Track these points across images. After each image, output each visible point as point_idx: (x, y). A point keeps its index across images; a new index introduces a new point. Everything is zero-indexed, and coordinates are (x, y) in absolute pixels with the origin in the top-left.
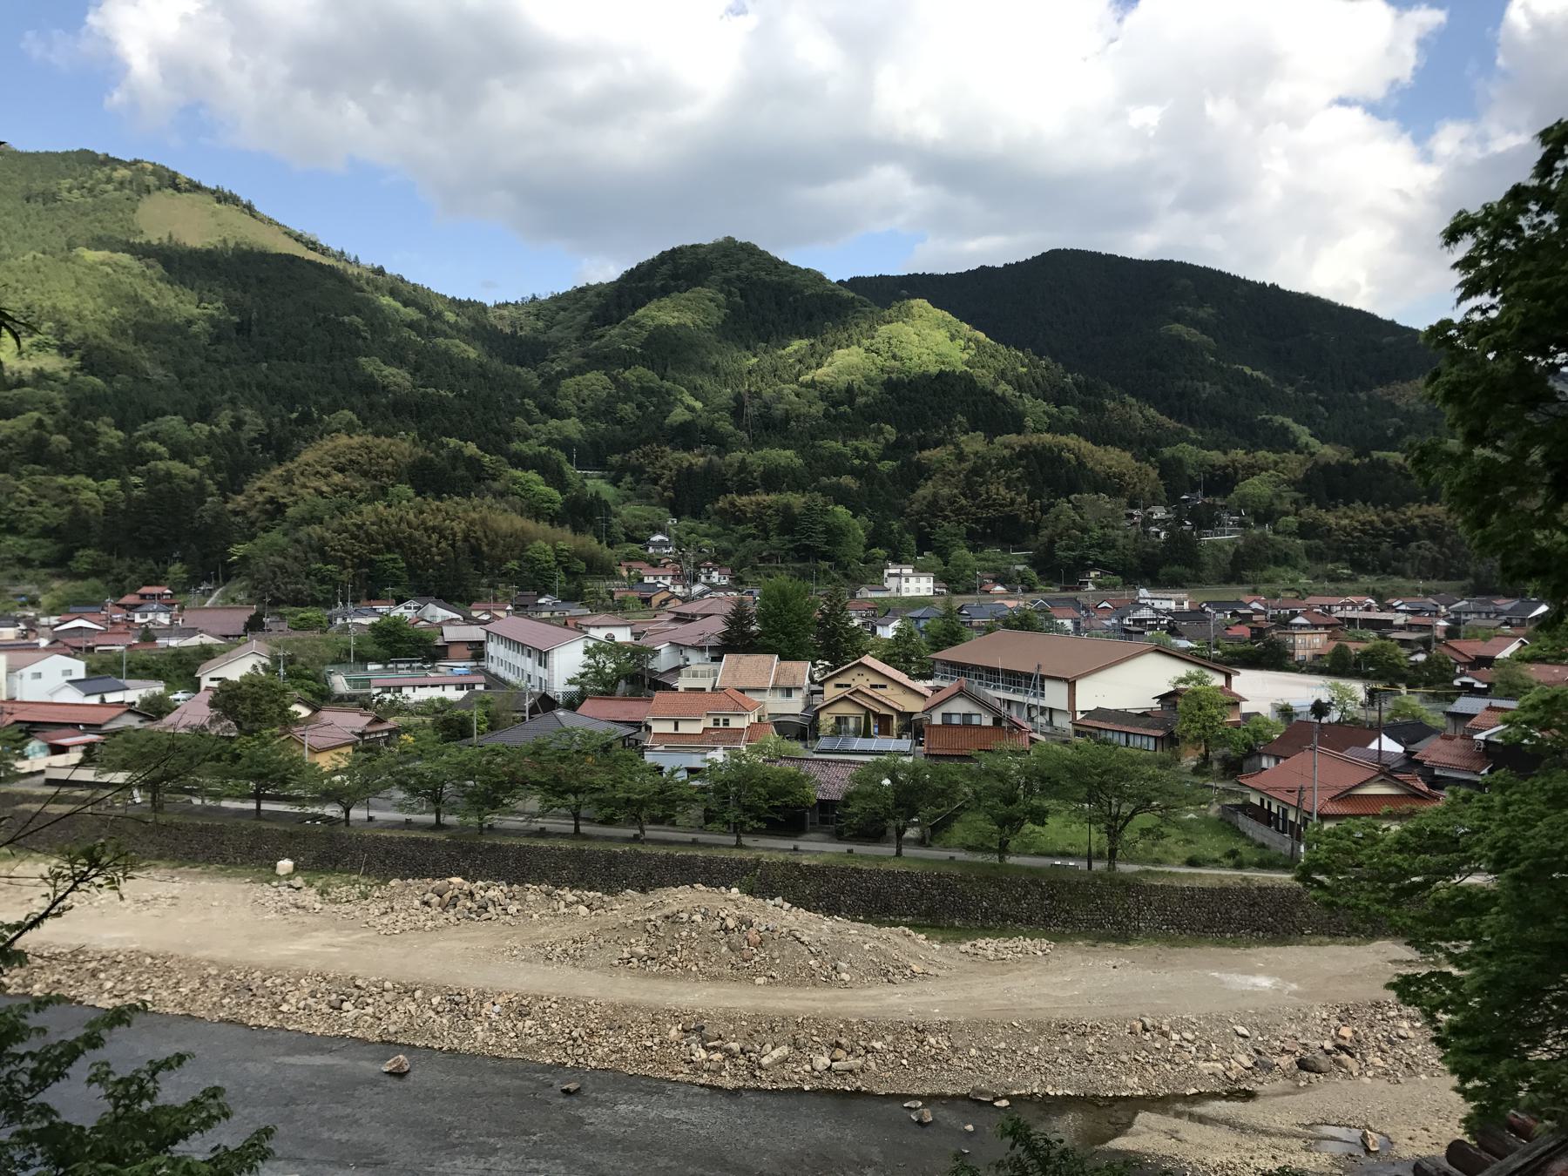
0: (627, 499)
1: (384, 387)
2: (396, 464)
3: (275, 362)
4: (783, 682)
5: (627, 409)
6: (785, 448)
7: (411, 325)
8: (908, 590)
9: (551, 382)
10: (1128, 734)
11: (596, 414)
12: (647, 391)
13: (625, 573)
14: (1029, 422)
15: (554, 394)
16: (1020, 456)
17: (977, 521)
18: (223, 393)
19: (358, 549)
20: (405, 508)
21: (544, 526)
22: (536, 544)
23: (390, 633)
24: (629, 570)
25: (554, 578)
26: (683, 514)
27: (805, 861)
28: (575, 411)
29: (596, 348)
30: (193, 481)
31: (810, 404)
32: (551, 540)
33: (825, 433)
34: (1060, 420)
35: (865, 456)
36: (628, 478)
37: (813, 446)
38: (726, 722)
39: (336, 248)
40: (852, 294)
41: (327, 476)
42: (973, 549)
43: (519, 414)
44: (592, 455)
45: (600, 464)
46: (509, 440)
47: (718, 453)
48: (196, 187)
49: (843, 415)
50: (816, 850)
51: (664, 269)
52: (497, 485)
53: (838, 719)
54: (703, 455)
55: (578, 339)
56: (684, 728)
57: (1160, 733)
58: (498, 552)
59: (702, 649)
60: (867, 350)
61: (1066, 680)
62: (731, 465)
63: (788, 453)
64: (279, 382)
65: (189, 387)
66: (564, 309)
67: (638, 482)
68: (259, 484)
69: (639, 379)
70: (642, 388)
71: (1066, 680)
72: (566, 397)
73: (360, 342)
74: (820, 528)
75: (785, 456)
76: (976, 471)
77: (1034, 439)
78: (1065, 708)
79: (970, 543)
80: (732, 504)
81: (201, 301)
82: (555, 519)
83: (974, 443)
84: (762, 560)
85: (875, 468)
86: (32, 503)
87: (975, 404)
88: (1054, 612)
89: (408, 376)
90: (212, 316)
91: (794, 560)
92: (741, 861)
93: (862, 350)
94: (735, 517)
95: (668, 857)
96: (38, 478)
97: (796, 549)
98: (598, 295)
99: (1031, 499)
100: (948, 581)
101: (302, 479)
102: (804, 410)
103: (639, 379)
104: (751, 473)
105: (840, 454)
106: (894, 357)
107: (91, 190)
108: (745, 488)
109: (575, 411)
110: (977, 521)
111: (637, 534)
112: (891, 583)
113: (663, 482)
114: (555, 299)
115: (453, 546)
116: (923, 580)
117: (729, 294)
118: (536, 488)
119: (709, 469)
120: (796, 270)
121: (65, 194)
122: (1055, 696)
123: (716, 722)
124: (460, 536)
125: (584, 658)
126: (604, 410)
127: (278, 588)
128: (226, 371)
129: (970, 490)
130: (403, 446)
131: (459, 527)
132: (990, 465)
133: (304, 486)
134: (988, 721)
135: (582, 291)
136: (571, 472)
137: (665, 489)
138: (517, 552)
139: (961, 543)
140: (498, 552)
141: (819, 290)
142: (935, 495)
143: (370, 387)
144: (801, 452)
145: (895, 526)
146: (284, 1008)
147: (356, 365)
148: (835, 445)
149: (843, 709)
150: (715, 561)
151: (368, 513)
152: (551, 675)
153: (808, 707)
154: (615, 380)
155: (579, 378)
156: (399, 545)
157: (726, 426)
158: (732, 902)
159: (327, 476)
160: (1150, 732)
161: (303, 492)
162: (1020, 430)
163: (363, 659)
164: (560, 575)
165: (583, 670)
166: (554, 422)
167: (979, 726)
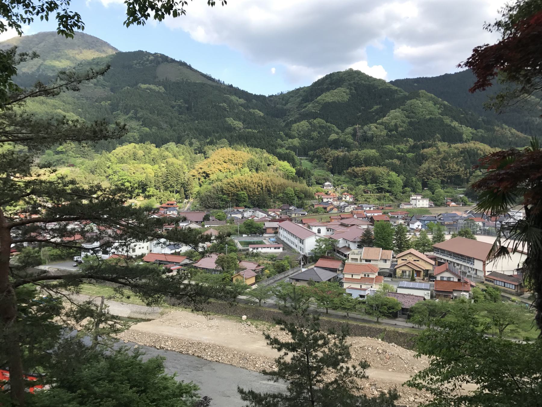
0: (315, 167)
1: (234, 128)
3: (200, 121)
4: (384, 258)
5: (315, 134)
7: (242, 105)
8: (419, 205)
9: (288, 125)
10: (505, 283)
12: (322, 127)
13: (317, 197)
14: (464, 136)
16: (462, 152)
17: (445, 177)
18: (185, 132)
19: (234, 190)
21: (290, 182)
23: (250, 225)
24: (318, 196)
25: (294, 199)
26: (335, 173)
27: (400, 330)
28: (297, 135)
29: (304, 112)
31: (381, 131)
34: (476, 135)
35: (402, 151)
36: (316, 160)
37: (383, 148)
38: (368, 275)
39: (217, 79)
40: (396, 88)
42: (443, 188)
44: (303, 152)
45: (306, 155)
46: (276, 148)
47: (348, 151)
48: (173, 61)
50: (402, 325)
51: (328, 81)
53: (403, 272)
54: (342, 151)
55: (297, 108)
56: (354, 277)
57: (517, 284)
58: (276, 191)
59: (355, 242)
60: (403, 110)
61: (482, 261)
62: (352, 155)
63: (374, 151)
64: (201, 127)
65: (174, 130)
66: (292, 97)
67: (319, 161)
69: (319, 123)
71: (482, 261)
72: (294, 131)
73: (226, 112)
74: (386, 181)
75: (372, 152)
76: (444, 158)
77: (466, 145)
78: (482, 270)
79: (442, 185)
80: (353, 170)
81: (176, 99)
82: (293, 179)
83: (443, 146)
85: (406, 156)
86: (134, 173)
87: (443, 130)
88: (475, 219)
91: (377, 193)
92: (380, 329)
93: (400, 110)
94: (355, 175)
95: (357, 325)
96: (136, 165)
97: (377, 189)
98: (304, 91)
99: (466, 169)
100: (433, 201)
103: (319, 123)
104: (360, 159)
105: (392, 151)
106: (413, 112)
107: (142, 64)
108: (358, 165)
109: (297, 135)
110: (445, 177)
111: (320, 182)
112: (413, 202)
113: (328, 162)
114: (289, 93)
115: (262, 189)
116: (425, 201)
117: (351, 89)
119: (344, 157)
120: (375, 80)
121: (135, 66)
122: (478, 265)
123: (365, 275)
124: (264, 186)
125: (316, 243)
126: (306, 135)
127: (209, 203)
128: (185, 124)
129: (442, 166)
131: (264, 182)
132: (450, 156)
134: (456, 280)
135: (298, 90)
136: (297, 158)
137: (329, 164)
138: (282, 191)
139: (439, 185)
141: (384, 87)
142: (429, 167)
143: (230, 129)
144: (378, 150)
145: (414, 179)
146: (257, 366)
147: (225, 121)
148: (390, 147)
149: (405, 268)
150: (347, 192)
152: (305, 246)
153: (393, 265)
154: (310, 123)
155: (298, 124)
156: (245, 189)
157: (350, 140)
158: (378, 343)
160: (513, 283)
162: (461, 141)
163: (241, 233)
164: (296, 198)
165: (316, 247)
166: (290, 140)
167: (453, 281)
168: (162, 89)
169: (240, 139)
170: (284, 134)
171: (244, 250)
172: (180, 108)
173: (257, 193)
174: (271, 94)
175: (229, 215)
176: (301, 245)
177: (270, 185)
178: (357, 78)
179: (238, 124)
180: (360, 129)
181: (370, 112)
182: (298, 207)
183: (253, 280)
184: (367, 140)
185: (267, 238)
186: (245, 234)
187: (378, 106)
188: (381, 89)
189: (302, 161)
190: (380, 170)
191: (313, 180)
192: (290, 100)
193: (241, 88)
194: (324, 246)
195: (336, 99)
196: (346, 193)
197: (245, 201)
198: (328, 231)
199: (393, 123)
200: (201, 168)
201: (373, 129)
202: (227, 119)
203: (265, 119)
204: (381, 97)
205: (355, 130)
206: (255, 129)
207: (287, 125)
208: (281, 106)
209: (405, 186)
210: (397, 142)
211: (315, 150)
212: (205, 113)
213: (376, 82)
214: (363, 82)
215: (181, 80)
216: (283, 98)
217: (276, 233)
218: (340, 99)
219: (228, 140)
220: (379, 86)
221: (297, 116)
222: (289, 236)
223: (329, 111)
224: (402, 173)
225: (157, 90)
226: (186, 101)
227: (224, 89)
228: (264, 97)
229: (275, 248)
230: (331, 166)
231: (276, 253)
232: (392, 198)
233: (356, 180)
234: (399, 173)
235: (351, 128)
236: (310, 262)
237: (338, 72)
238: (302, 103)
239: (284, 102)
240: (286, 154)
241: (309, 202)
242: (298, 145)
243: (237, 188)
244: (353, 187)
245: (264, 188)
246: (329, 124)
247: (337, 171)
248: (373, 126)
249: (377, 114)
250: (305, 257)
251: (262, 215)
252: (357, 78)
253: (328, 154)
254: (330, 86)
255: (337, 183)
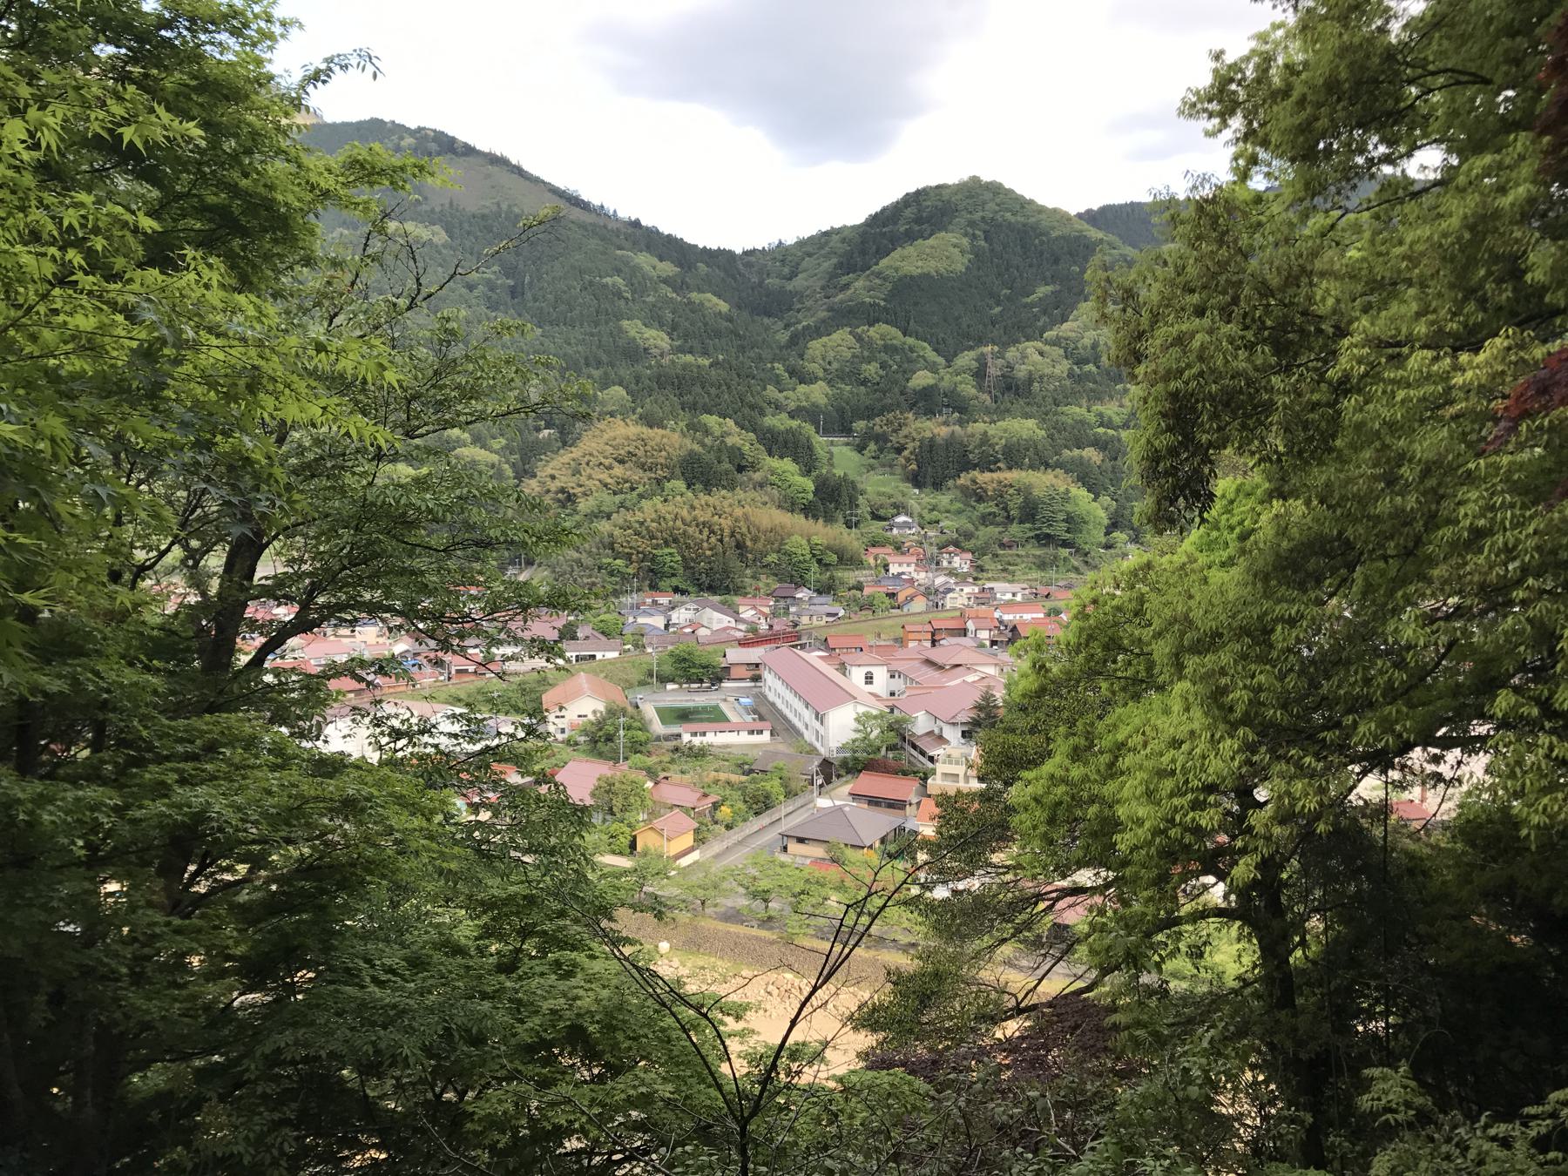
0: (872, 468)
2: (669, 457)
5: (871, 370)
6: (1027, 416)
7: (665, 281)
11: (842, 376)
12: (890, 349)
13: (872, 561)
15: (801, 356)
19: (643, 545)
20: (679, 505)
21: (799, 520)
22: (793, 538)
23: (685, 660)
29: (841, 302)
30: (493, 466)
32: (806, 533)
33: (1068, 397)
35: (1108, 424)
36: (872, 446)
37: (1056, 414)
39: (596, 202)
41: (610, 468)
43: (770, 381)
44: (838, 422)
45: (846, 430)
46: (762, 414)
47: (961, 422)
48: (469, 151)
49: (1088, 377)
51: (908, 212)
52: (757, 476)
54: (946, 423)
55: (823, 288)
58: (760, 545)
62: (973, 435)
63: (1031, 423)
66: (810, 255)
68: (549, 471)
70: (885, 346)
73: (622, 302)
74: (1061, 516)
75: (1025, 428)
80: (974, 481)
82: (809, 510)
84: (1002, 546)
85: (1119, 440)
89: (666, 337)
90: (490, 280)
98: (843, 240)
101: (589, 471)
102: (1048, 371)
105: (1082, 422)
108: (988, 464)
111: (882, 512)
113: (906, 453)
114: (801, 243)
115: (721, 541)
117: (974, 237)
118: (790, 478)
119: (951, 442)
120: (1042, 210)
124: (727, 532)
125: (855, 725)
126: (848, 373)
130: (673, 440)
131: (726, 523)
133: (590, 477)
136: (820, 441)
137: (907, 460)
140: (760, 545)
141: (1066, 231)
143: (635, 353)
147: (620, 330)
148: (1076, 411)
151: (649, 509)
152: (827, 729)
154: (859, 339)
155: (825, 339)
156: (675, 541)
157: (968, 389)
159: (610, 468)
161: (589, 483)
163: (664, 680)
164: (815, 567)
166: (802, 388)
168: (440, 236)
169: (661, 386)
170: (786, 370)
171: (667, 738)
172: (492, 290)
173: (708, 553)
174: (749, 247)
175: (631, 619)
176: (817, 725)
177: (744, 530)
178: (991, 206)
179: (657, 339)
180: (996, 356)
181: (1026, 305)
182: (819, 592)
183: (688, 840)
184: (1014, 391)
185: (730, 698)
186: (673, 681)
187: (1050, 288)
188: (1056, 238)
189: (835, 450)
190: (1042, 482)
191: (864, 510)
192: (804, 264)
193: (665, 229)
194: (876, 732)
195: (931, 266)
196: (951, 548)
197: (674, 575)
198: (892, 677)
199: (1087, 341)
200: (553, 477)
201: (1033, 358)
202: (625, 323)
203: (730, 320)
204: (1056, 261)
205: (982, 360)
206: (705, 353)
207: (794, 341)
208: (777, 281)
209: (1114, 525)
210: (1097, 397)
211: (869, 418)
212: (563, 307)
213: (1043, 216)
214: (1008, 215)
215: (494, 208)
216: (786, 258)
217: (756, 679)
218: (942, 266)
219: (626, 388)
220: (1053, 228)
221: (823, 314)
222: (789, 696)
223: (910, 303)
224: (1106, 489)
225: (425, 238)
226: (509, 271)
227: (617, 233)
228: (730, 253)
229: (751, 732)
230: (914, 467)
231: (756, 746)
232: (1075, 562)
233: (982, 508)
234: (1094, 490)
235: (972, 354)
236: (839, 776)
237: (938, 187)
238: (837, 276)
239: (786, 270)
240: (790, 431)
241: (851, 576)
242: (822, 401)
243: (652, 537)
244: (970, 527)
245: (726, 539)
246: (910, 341)
247: (929, 480)
248: (1031, 347)
249: (1045, 312)
250: (826, 764)
251: (720, 621)
252: (991, 206)
253: (905, 431)
254: (917, 228)
255: (928, 517)
